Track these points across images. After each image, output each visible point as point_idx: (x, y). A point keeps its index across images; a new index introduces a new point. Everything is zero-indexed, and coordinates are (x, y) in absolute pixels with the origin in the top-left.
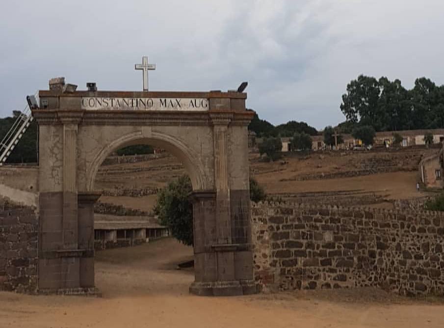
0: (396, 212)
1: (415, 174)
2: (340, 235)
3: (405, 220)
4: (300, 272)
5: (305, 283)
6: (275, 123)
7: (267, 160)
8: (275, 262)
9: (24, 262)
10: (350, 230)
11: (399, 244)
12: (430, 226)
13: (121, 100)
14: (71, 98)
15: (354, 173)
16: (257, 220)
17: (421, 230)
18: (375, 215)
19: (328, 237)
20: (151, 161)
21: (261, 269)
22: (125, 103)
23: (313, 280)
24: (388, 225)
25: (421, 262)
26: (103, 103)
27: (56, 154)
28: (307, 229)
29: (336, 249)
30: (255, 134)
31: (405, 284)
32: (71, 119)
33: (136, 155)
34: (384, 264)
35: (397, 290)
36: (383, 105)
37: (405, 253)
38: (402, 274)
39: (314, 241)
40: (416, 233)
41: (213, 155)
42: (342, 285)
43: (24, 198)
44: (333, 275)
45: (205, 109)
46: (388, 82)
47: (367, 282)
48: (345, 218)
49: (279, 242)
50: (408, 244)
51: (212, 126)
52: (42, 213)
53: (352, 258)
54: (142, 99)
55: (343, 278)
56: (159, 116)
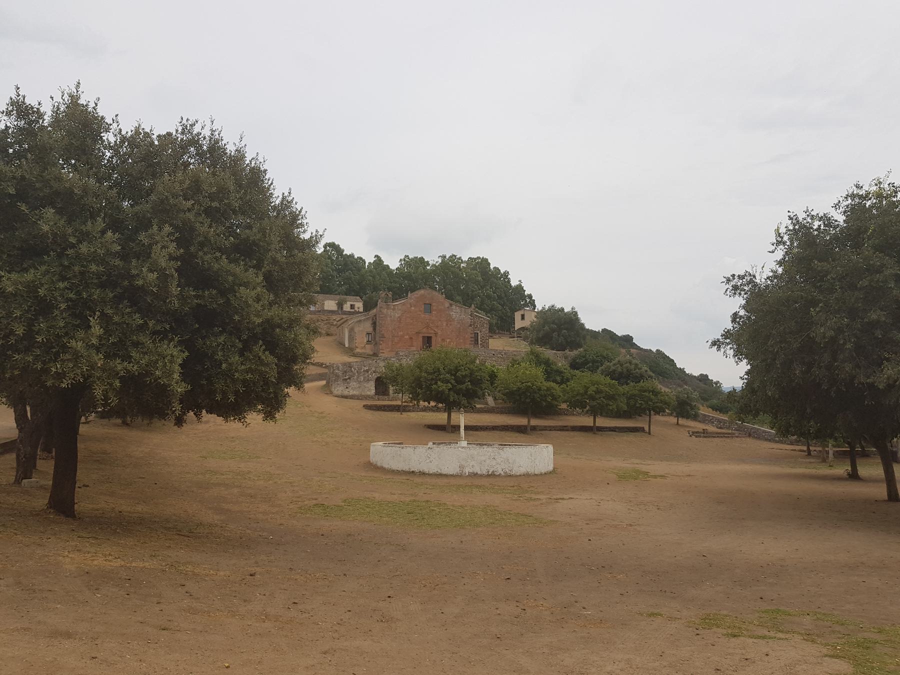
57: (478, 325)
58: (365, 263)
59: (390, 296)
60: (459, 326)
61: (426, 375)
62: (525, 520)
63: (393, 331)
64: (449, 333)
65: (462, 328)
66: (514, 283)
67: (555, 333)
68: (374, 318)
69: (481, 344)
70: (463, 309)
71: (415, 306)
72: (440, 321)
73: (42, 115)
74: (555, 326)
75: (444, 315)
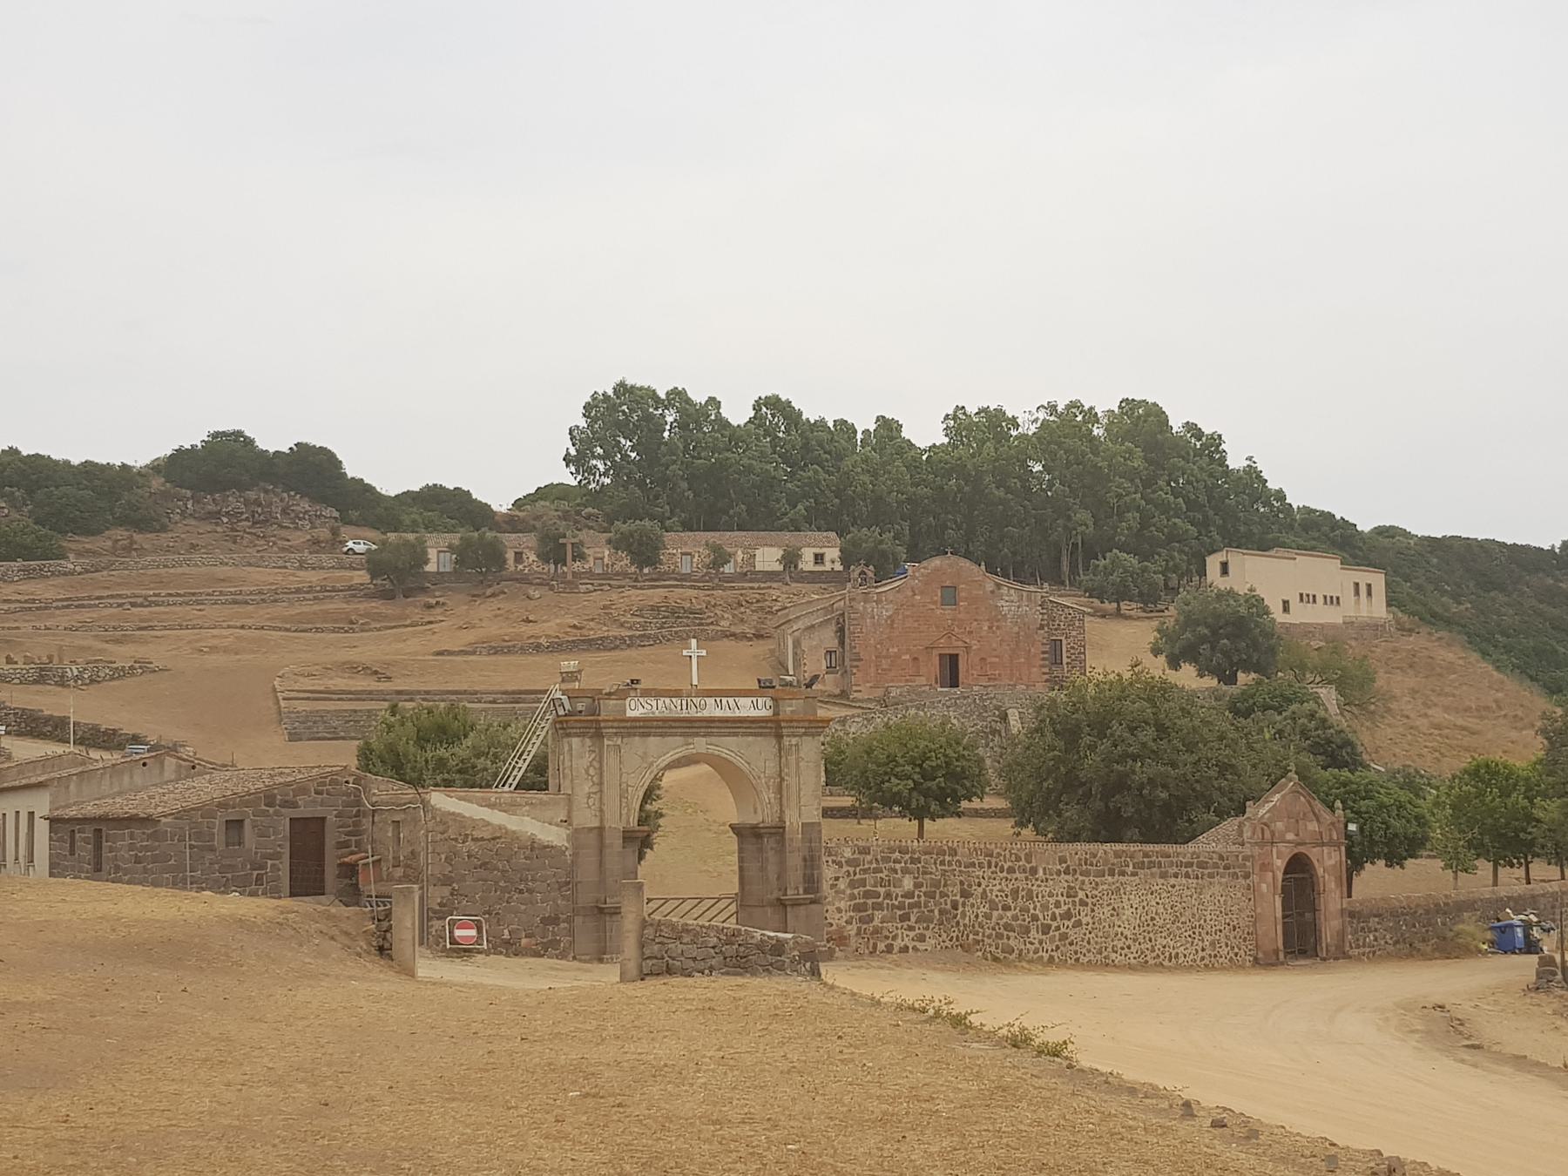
0: (982, 846)
1: (761, 648)
2: (920, 880)
3: (991, 856)
4: (877, 931)
5: (881, 946)
6: (390, 484)
7: (387, 596)
8: (852, 917)
9: (554, 920)
10: (931, 873)
11: (984, 891)
12: (1021, 863)
13: (667, 700)
14: (615, 702)
15: (618, 642)
16: (830, 863)
17: (1011, 870)
18: (960, 851)
19: (908, 883)
20: (61, 580)
21: (834, 927)
22: (672, 706)
23: (890, 941)
24: (973, 865)
25: (1009, 914)
26: (646, 705)
27: (592, 776)
28: (886, 872)
29: (916, 899)
30: (336, 514)
31: (990, 945)
32: (614, 730)
33: (20, 563)
34: (967, 918)
35: (980, 954)
36: (674, 462)
37: (991, 901)
38: (988, 932)
39: (892, 889)
40: (1005, 874)
41: (780, 775)
42: (921, 948)
43: (554, 836)
44: (912, 934)
45: (769, 713)
46: (688, 401)
47: (948, 944)
48: (927, 857)
49: (856, 891)
50: (995, 889)
51: (779, 737)
52: (575, 855)
53: (932, 911)
54: (694, 699)
55: (922, 938)
56: (718, 724)
57: (1062, 624)
58: (855, 432)
59: (871, 574)
60: (1016, 629)
61: (874, 767)
63: (879, 646)
64: (994, 645)
65: (1022, 633)
66: (1235, 462)
67: (1205, 646)
68: (841, 620)
69: (1067, 663)
70: (1025, 594)
71: (922, 593)
72: (976, 620)
74: (1206, 631)
75: (983, 609)
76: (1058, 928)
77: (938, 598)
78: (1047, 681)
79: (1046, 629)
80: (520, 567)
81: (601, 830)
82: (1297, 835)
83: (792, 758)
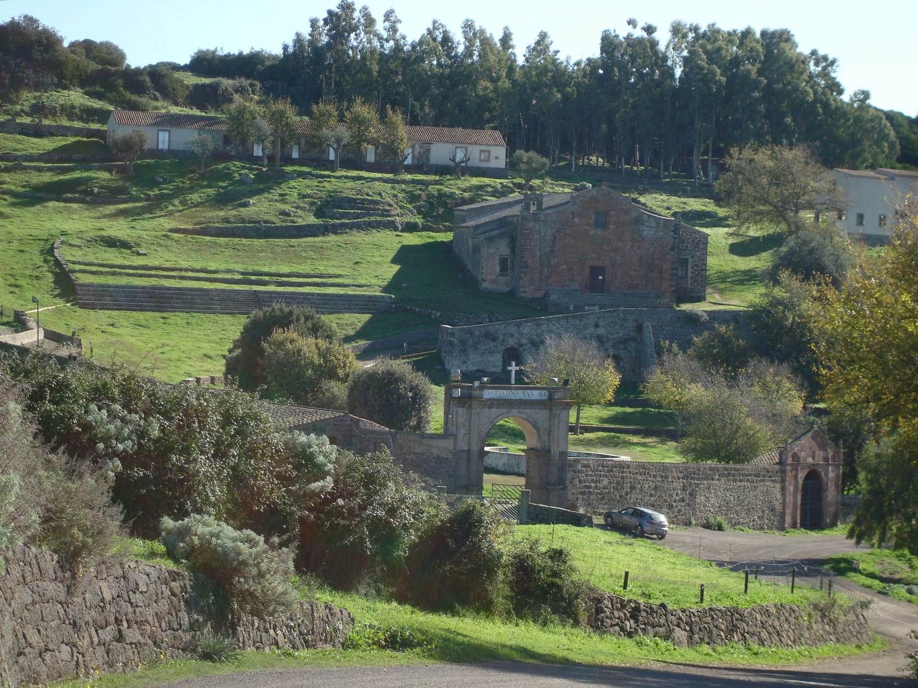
51: (550, 410)
57: (689, 245)
62: (216, 318)
69: (692, 278)
71: (580, 216)
72: (621, 241)
73: (769, 94)
76: (677, 506)
77: (592, 221)
78: (674, 292)
79: (676, 250)
80: (228, 148)
81: (469, 451)
82: (814, 459)
83: (556, 420)
